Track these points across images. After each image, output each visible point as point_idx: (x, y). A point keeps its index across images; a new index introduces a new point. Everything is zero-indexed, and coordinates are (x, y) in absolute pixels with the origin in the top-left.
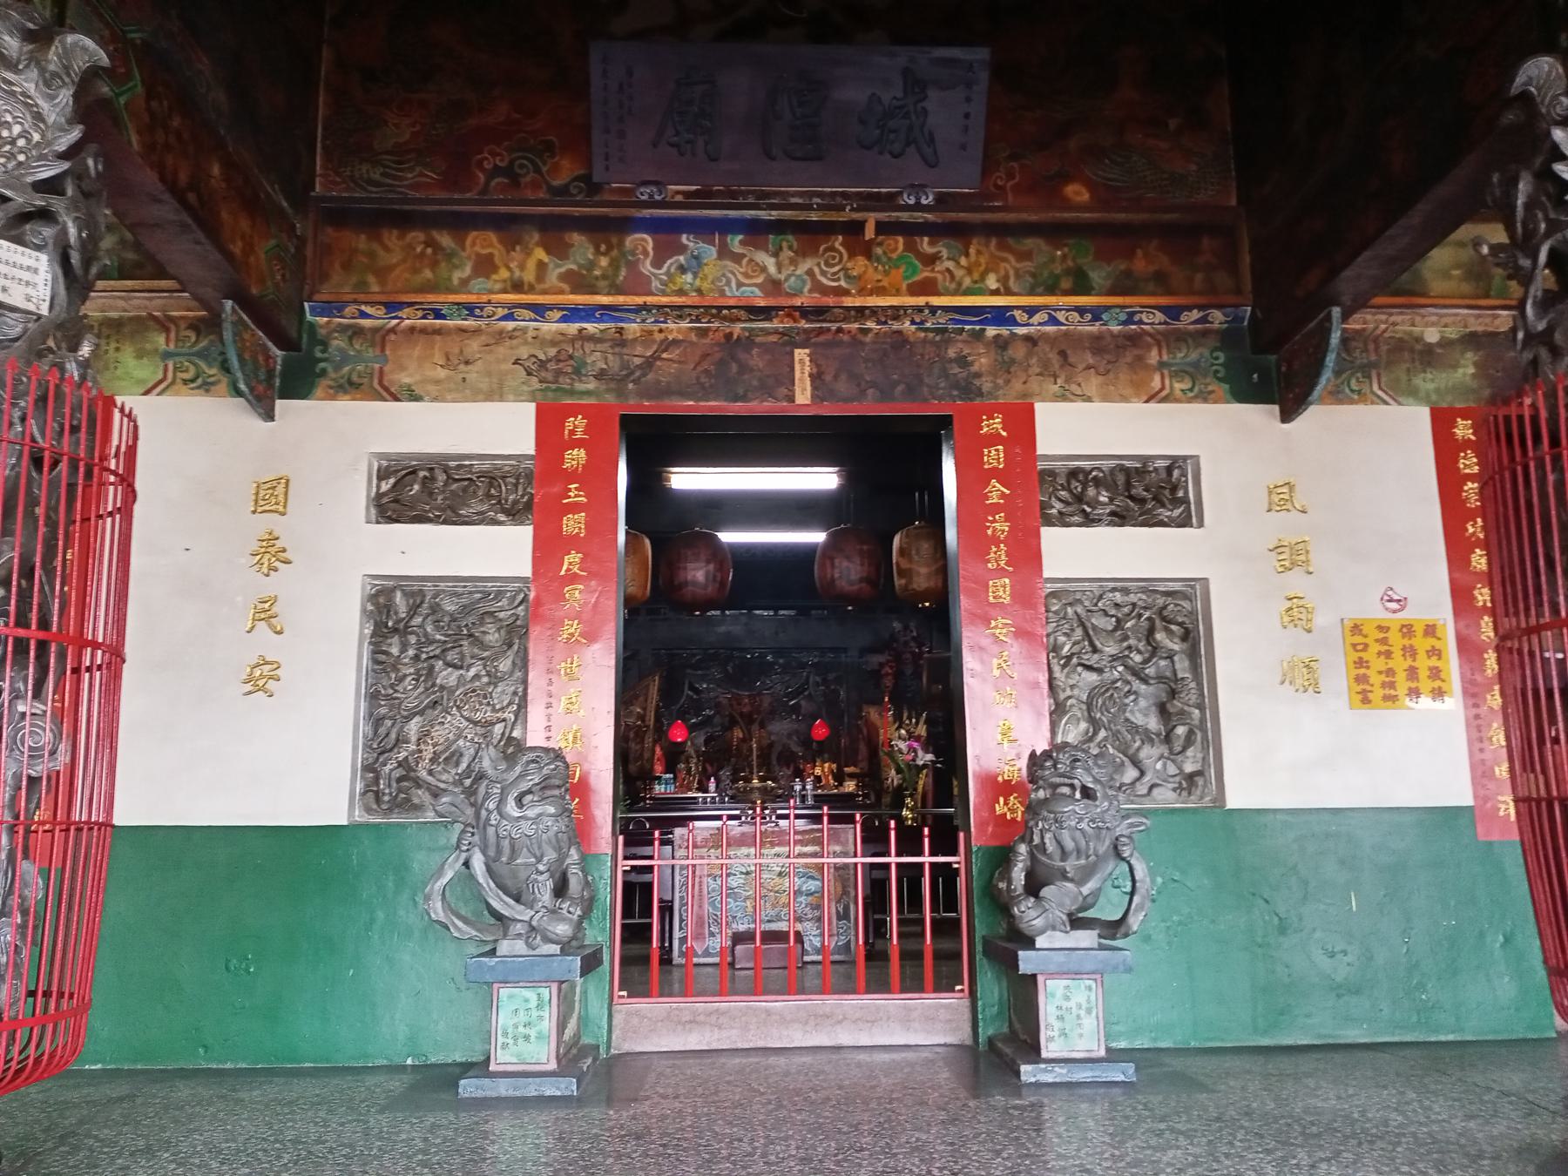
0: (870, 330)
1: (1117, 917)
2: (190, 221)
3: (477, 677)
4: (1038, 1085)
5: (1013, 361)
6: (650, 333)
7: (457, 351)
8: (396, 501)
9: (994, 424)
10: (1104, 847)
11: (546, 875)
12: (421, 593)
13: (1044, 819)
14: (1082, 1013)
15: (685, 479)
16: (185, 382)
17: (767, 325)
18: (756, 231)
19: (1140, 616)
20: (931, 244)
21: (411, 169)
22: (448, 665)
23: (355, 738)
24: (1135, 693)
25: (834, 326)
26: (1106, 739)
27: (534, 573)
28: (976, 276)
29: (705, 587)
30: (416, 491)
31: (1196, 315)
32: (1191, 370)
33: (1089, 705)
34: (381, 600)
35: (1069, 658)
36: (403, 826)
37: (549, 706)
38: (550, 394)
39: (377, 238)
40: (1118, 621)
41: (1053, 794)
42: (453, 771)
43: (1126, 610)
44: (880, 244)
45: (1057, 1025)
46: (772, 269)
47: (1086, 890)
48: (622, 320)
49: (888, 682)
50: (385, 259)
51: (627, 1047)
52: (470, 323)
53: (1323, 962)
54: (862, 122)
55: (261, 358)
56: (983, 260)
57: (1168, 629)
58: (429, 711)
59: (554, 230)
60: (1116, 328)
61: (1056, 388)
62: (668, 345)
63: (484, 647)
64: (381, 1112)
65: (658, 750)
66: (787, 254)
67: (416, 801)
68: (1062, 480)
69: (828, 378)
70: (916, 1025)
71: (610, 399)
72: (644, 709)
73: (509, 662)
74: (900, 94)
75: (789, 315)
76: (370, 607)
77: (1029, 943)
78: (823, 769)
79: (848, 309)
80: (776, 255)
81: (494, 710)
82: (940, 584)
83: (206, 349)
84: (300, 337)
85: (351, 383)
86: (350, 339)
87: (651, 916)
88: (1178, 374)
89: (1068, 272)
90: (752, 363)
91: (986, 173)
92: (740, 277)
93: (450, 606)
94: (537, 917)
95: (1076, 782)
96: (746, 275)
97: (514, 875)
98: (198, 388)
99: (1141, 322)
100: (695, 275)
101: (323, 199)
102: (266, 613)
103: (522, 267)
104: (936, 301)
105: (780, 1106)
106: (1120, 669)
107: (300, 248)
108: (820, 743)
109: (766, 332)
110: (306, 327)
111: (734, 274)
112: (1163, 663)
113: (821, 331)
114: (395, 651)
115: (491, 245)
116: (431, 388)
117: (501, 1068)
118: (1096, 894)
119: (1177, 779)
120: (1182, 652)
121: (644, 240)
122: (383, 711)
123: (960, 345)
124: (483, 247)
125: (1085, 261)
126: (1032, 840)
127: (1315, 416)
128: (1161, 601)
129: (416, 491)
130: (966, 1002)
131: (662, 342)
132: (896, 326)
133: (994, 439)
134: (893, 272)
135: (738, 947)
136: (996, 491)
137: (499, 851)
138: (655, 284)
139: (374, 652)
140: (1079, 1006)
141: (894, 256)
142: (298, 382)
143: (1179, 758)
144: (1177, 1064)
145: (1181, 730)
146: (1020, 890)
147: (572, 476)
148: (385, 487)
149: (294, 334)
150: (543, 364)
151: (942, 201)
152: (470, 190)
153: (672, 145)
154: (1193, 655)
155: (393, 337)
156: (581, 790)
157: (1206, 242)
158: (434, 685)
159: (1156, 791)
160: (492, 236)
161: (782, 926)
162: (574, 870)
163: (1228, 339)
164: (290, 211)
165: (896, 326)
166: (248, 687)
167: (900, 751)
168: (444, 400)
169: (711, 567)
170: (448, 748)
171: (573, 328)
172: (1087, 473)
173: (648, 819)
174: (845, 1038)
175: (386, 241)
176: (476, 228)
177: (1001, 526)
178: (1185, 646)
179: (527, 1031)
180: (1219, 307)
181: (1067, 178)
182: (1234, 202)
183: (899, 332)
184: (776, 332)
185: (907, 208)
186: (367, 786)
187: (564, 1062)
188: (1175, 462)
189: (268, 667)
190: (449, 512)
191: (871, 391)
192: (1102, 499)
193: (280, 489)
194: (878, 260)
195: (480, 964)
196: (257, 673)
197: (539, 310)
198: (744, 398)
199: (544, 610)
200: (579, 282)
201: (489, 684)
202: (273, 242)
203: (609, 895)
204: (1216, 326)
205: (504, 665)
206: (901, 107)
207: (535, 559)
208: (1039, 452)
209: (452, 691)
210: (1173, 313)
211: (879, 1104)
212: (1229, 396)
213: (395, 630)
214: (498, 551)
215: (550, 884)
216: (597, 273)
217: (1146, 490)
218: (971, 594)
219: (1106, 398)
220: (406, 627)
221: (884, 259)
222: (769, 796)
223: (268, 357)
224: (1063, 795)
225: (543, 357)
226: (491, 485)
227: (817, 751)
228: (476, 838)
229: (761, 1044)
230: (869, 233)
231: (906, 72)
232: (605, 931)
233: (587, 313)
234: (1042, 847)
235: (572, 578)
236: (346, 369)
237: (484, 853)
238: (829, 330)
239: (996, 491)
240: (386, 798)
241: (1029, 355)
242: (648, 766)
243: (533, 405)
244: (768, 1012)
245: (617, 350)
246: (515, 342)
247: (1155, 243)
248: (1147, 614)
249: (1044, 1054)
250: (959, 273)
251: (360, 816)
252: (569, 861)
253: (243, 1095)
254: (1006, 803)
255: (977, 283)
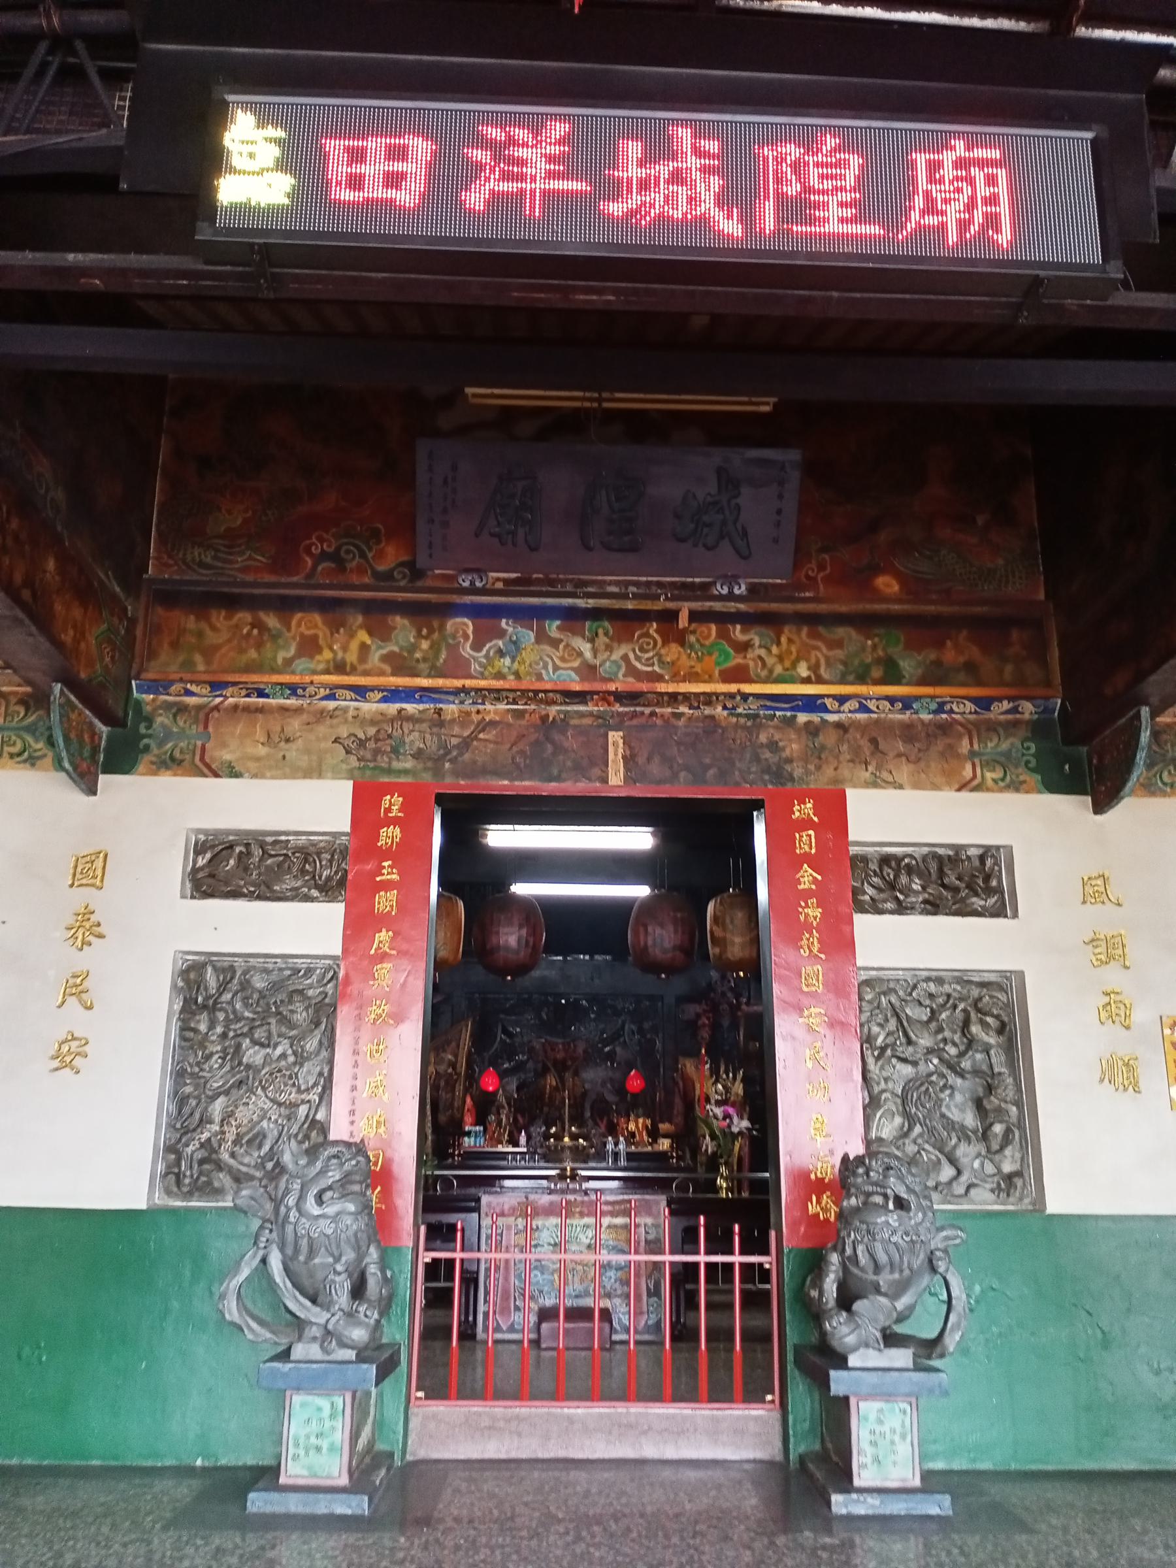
0: (682, 714)
1: (933, 1335)
2: (21, 614)
3: (283, 1056)
4: (850, 1518)
5: (823, 747)
6: (468, 714)
7: (279, 729)
8: (212, 876)
9: (805, 810)
10: (919, 1261)
11: (344, 1276)
12: (232, 969)
13: (857, 1230)
14: (897, 1438)
15: (501, 837)
16: (12, 756)
17: (582, 708)
18: (573, 618)
19: (955, 1007)
20: (743, 631)
21: (241, 553)
22: (255, 1043)
23: (159, 1116)
24: (951, 1087)
25: (647, 711)
26: (921, 1135)
27: (345, 950)
28: (787, 664)
29: (517, 952)
30: (228, 867)
31: (1006, 705)
32: (1003, 759)
33: (904, 1098)
34: (192, 976)
35: (883, 1050)
36: (202, 1211)
37: (354, 1088)
38: (368, 773)
39: (207, 619)
40: (933, 1011)
41: (865, 1203)
42: (256, 1154)
43: (941, 1000)
44: (693, 632)
45: (869, 1450)
46: (588, 655)
47: (901, 1304)
48: (441, 701)
49: (705, 1034)
50: (212, 638)
51: (422, 1454)
52: (292, 702)
53: (1150, 1380)
54: (677, 516)
55: (86, 737)
56: (793, 649)
57: (983, 1026)
58: (234, 1091)
59: (377, 613)
60: (926, 717)
61: (868, 775)
62: (484, 726)
63: (292, 1026)
64: (165, 1528)
65: (468, 1100)
66: (602, 640)
67: (216, 1184)
68: (874, 866)
69: (641, 760)
70: (728, 1436)
71: (427, 777)
72: (456, 1056)
73: (315, 1042)
74: (714, 491)
75: (604, 699)
76: (180, 984)
77: (841, 1361)
78: (636, 1124)
79: (661, 694)
80: (592, 641)
81: (299, 1091)
82: (754, 954)
83: (34, 723)
84: (126, 714)
85: (172, 758)
86: (175, 716)
87: (453, 1280)
88: (989, 764)
89: (878, 661)
90: (566, 744)
91: (797, 566)
92: (558, 662)
93: (259, 983)
94: (334, 1320)
95: (889, 1191)
96: (563, 659)
97: (311, 1275)
98: (25, 761)
99: (952, 711)
100: (513, 660)
101: (151, 581)
102: (77, 989)
103: (345, 649)
104: (747, 688)
105: (578, 1539)
106: (936, 1061)
107: (130, 630)
108: (635, 1096)
109: (582, 715)
110: (132, 703)
111: (552, 659)
112: (979, 1056)
113: (634, 715)
114: (203, 1027)
115: (316, 626)
116: (252, 765)
117: (290, 1482)
118: (911, 1308)
119: (996, 1179)
120: (999, 1045)
121: (465, 624)
122: (188, 1089)
123: (772, 731)
124: (308, 628)
125: (896, 651)
126: (844, 1250)
127: (1131, 810)
128: (975, 992)
129: (228, 867)
130: (776, 1415)
131: (479, 723)
132: (708, 711)
133: (806, 824)
134: (706, 658)
135: (544, 1326)
136: (807, 877)
137: (297, 1250)
138: (475, 667)
139: (182, 1029)
140: (893, 1431)
141: (707, 643)
142: (122, 757)
143: (997, 1157)
144: (995, 1491)
145: (998, 1128)
146: (832, 1303)
147: (385, 854)
148: (201, 862)
149: (121, 714)
150: (362, 743)
151: (753, 590)
152: (297, 574)
153: (492, 535)
154: (1010, 1048)
155: (216, 714)
156: (382, 1178)
157: (1015, 634)
158: (240, 1064)
159: (973, 1192)
160: (317, 618)
161: (588, 1302)
162: (373, 1269)
163: (1038, 729)
164: (122, 595)
165: (708, 711)
166: (56, 1064)
167: (715, 1117)
168: (263, 777)
169: (524, 932)
170: (251, 1130)
171: (392, 708)
172: (899, 859)
173: (456, 1177)
174: (650, 1451)
175: (214, 620)
176: (302, 610)
177: (813, 912)
178: (1001, 1039)
179: (319, 1442)
180: (1028, 698)
181: (876, 570)
182: (1042, 596)
183: (712, 717)
184: (591, 714)
185: (721, 598)
186: (168, 1167)
187: (356, 1475)
188: (987, 852)
189: (74, 1044)
190: (263, 887)
191: (682, 774)
192: (915, 887)
193: (99, 863)
194: (691, 647)
195: (274, 1373)
196: (65, 1048)
197: (361, 692)
198: (558, 779)
199: (354, 989)
200: (400, 664)
201: (295, 1063)
202: (104, 627)
203: (410, 1287)
204: (1027, 716)
205: (311, 1044)
206: (715, 503)
207: (346, 938)
208: (851, 838)
209: (257, 1071)
210: (984, 704)
211: (682, 1539)
212: (1041, 787)
213: (204, 1007)
214: (308, 929)
215: (347, 1285)
216: (418, 655)
217: (959, 878)
218: (784, 980)
219: (917, 786)
220: (215, 1003)
221: (697, 646)
222: (581, 1156)
223: (93, 733)
224: (876, 1205)
225: (361, 735)
226: (306, 861)
227: (632, 1105)
228: (274, 1235)
229: (562, 1454)
230: (683, 621)
231: (720, 471)
232: (403, 1330)
233: (408, 694)
234: (855, 1259)
235: (382, 957)
236: (170, 745)
237: (282, 1249)
238: (642, 713)
239: (807, 877)
240: (187, 1181)
241: (841, 741)
242: (458, 1115)
243: (351, 783)
244: (570, 1420)
245: (435, 730)
246: (335, 721)
247: (965, 633)
248: (961, 1006)
249: (857, 1482)
250: (770, 661)
251: (160, 1199)
252: (367, 1260)
253: (25, 1502)
254: (819, 1202)
255: (791, 674)
